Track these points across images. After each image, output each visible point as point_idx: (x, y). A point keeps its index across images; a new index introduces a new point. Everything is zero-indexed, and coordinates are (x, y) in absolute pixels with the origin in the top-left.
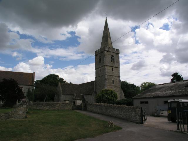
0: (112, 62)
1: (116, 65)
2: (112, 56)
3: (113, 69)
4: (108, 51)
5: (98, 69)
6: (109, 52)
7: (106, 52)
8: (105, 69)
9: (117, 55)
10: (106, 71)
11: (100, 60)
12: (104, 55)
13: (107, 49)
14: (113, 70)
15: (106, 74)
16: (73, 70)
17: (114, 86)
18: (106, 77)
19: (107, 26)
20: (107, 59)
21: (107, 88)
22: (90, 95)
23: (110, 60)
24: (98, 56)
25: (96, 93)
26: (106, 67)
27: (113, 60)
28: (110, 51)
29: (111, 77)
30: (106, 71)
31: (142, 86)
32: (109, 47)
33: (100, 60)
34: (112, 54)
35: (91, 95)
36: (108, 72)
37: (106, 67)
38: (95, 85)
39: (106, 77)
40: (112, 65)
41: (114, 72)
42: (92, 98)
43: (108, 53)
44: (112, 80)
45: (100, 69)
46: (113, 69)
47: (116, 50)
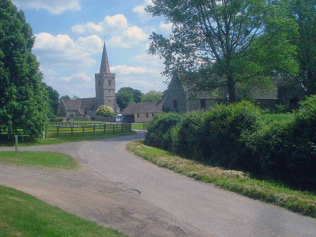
20: (106, 82)
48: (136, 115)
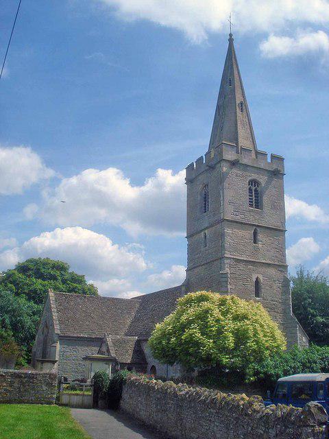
0: (251, 205)
2: (254, 182)
8: (222, 235)
13: (230, 155)
32: (240, 145)
41: (260, 246)
43: (235, 170)
47: (269, 160)
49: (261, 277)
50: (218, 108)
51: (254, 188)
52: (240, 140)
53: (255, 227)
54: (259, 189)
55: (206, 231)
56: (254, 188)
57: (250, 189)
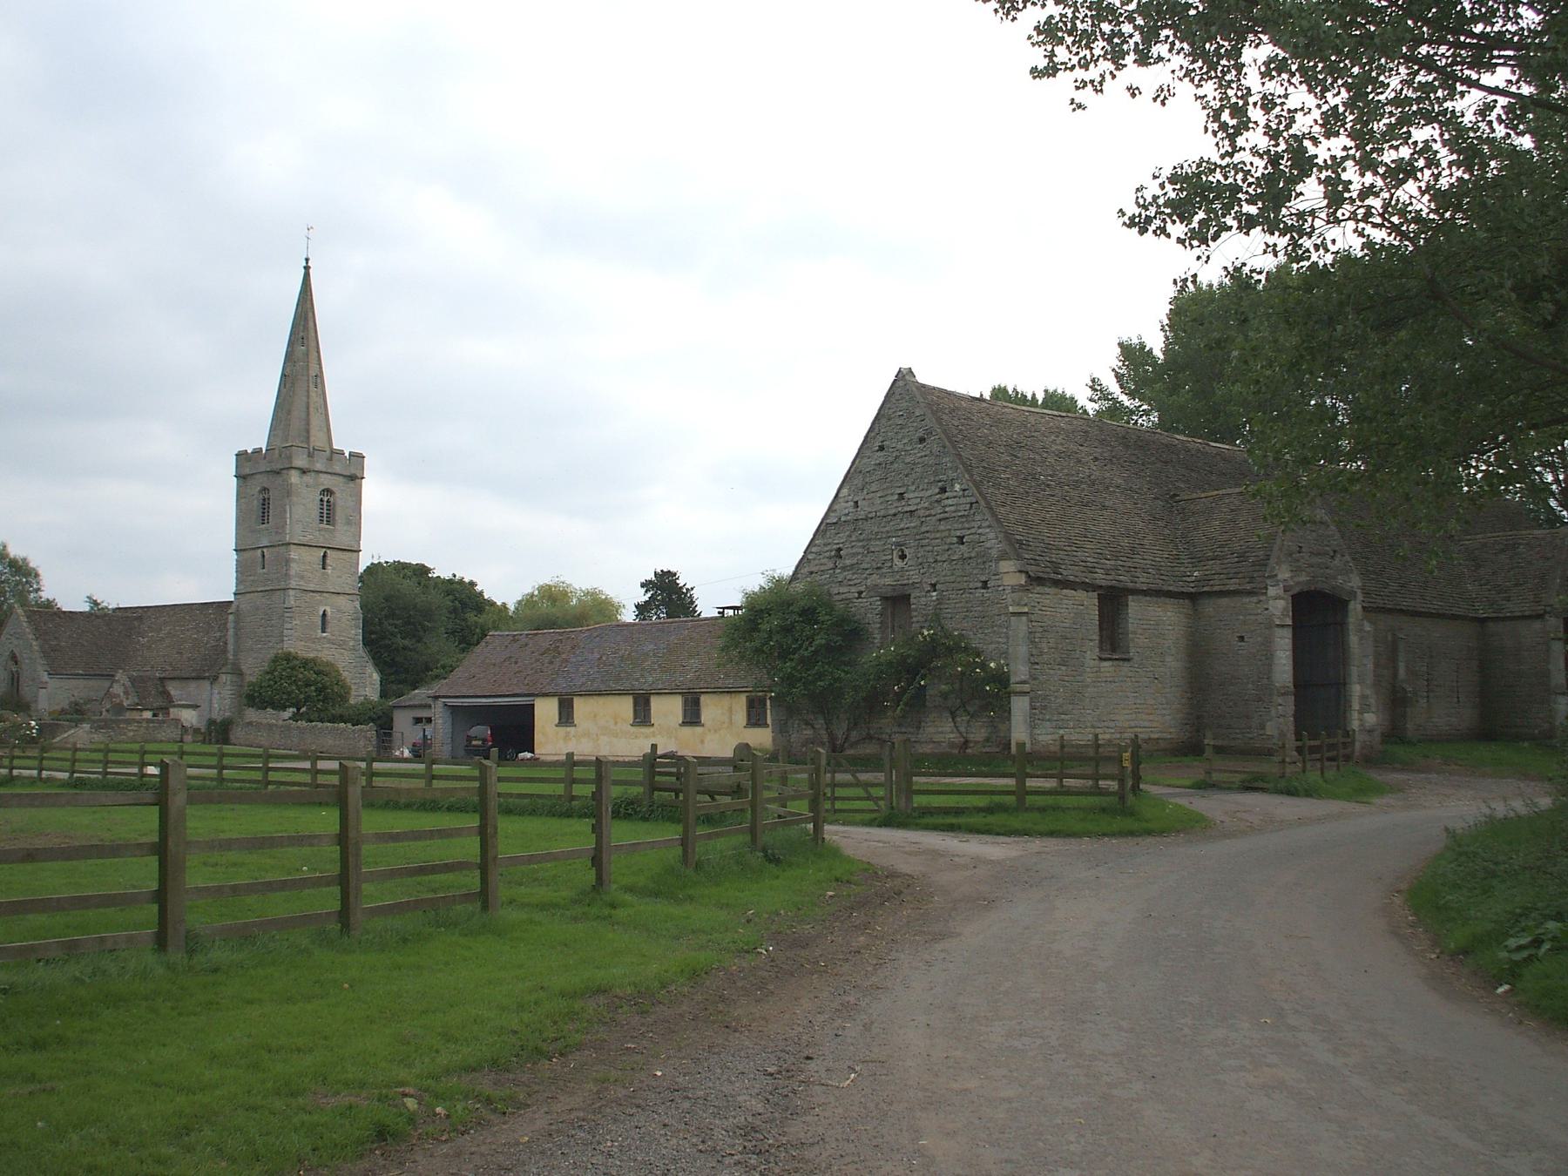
1: (341, 537)
2: (328, 491)
3: (325, 556)
4: (304, 472)
5: (248, 555)
6: (313, 474)
7: (294, 477)
8: (288, 561)
9: (352, 485)
10: (292, 572)
11: (265, 504)
12: (288, 492)
14: (328, 562)
15: (293, 584)
16: (292, 650)
17: (330, 641)
18: (291, 602)
19: (306, 319)
20: (301, 511)
21: (296, 645)
22: (206, 684)
23: (316, 513)
24: (254, 488)
25: (237, 672)
26: (295, 554)
27: (328, 513)
28: (319, 466)
29: (317, 596)
30: (294, 568)
31: (528, 602)
33: (265, 504)
34: (326, 481)
35: (215, 679)
36: (302, 578)
37: (295, 554)
38: (231, 632)
39: (291, 602)
40: (321, 539)
41: (330, 571)
42: (875, 599)
43: (308, 478)
44: (321, 613)
45: (263, 556)
46: (325, 556)
48: (546, 711)
49: (329, 610)
50: (284, 375)
51: (326, 499)
52: (312, 439)
53: (324, 550)
54: (332, 499)
55: (265, 550)
56: (326, 499)
57: (322, 500)
